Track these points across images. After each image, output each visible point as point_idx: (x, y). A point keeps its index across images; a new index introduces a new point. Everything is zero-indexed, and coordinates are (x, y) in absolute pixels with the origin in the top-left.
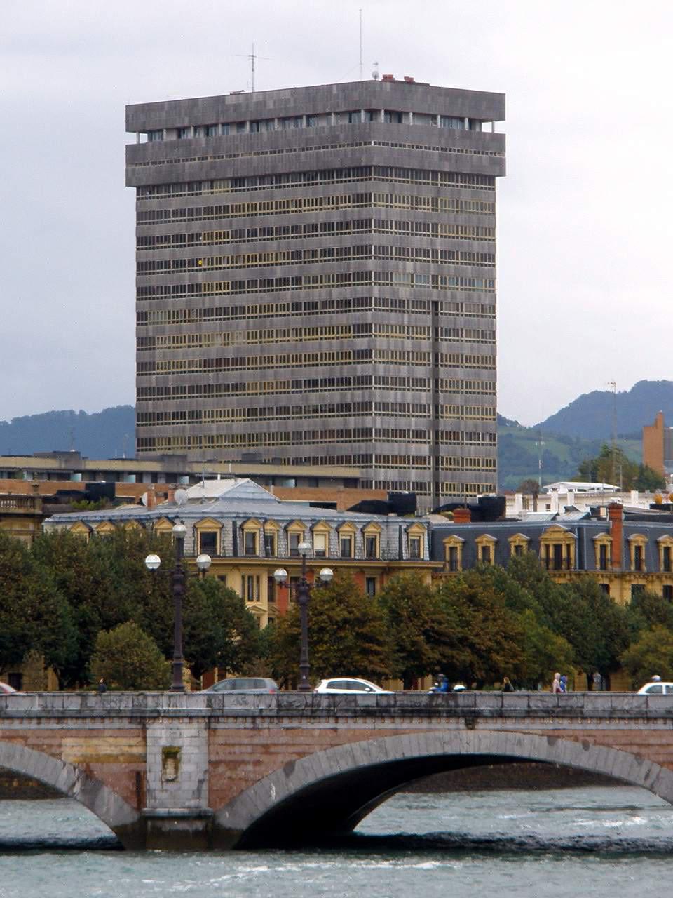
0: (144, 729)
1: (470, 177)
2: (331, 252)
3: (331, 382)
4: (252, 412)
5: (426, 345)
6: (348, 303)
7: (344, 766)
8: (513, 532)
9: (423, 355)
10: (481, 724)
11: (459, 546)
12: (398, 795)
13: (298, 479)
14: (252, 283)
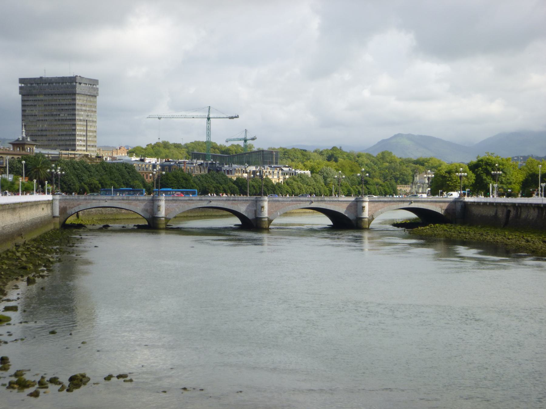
1: (92, 96)
2: (67, 110)
3: (67, 135)
4: (49, 140)
5: (85, 128)
6: (71, 120)
9: (84, 130)
14: (49, 115)
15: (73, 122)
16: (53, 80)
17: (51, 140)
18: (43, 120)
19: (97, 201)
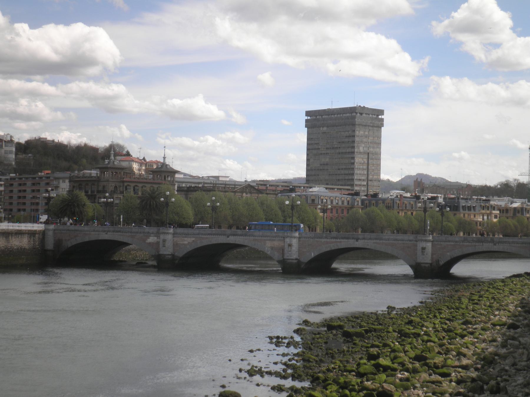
0: (284, 240)
3: (346, 169)
4: (330, 175)
7: (328, 249)
8: (379, 200)
10: (359, 241)
11: (368, 203)
12: (463, 260)
13: (337, 189)
14: (330, 148)
15: (351, 156)
16: (335, 111)
17: (332, 175)
18: (325, 154)
19: (96, 233)
